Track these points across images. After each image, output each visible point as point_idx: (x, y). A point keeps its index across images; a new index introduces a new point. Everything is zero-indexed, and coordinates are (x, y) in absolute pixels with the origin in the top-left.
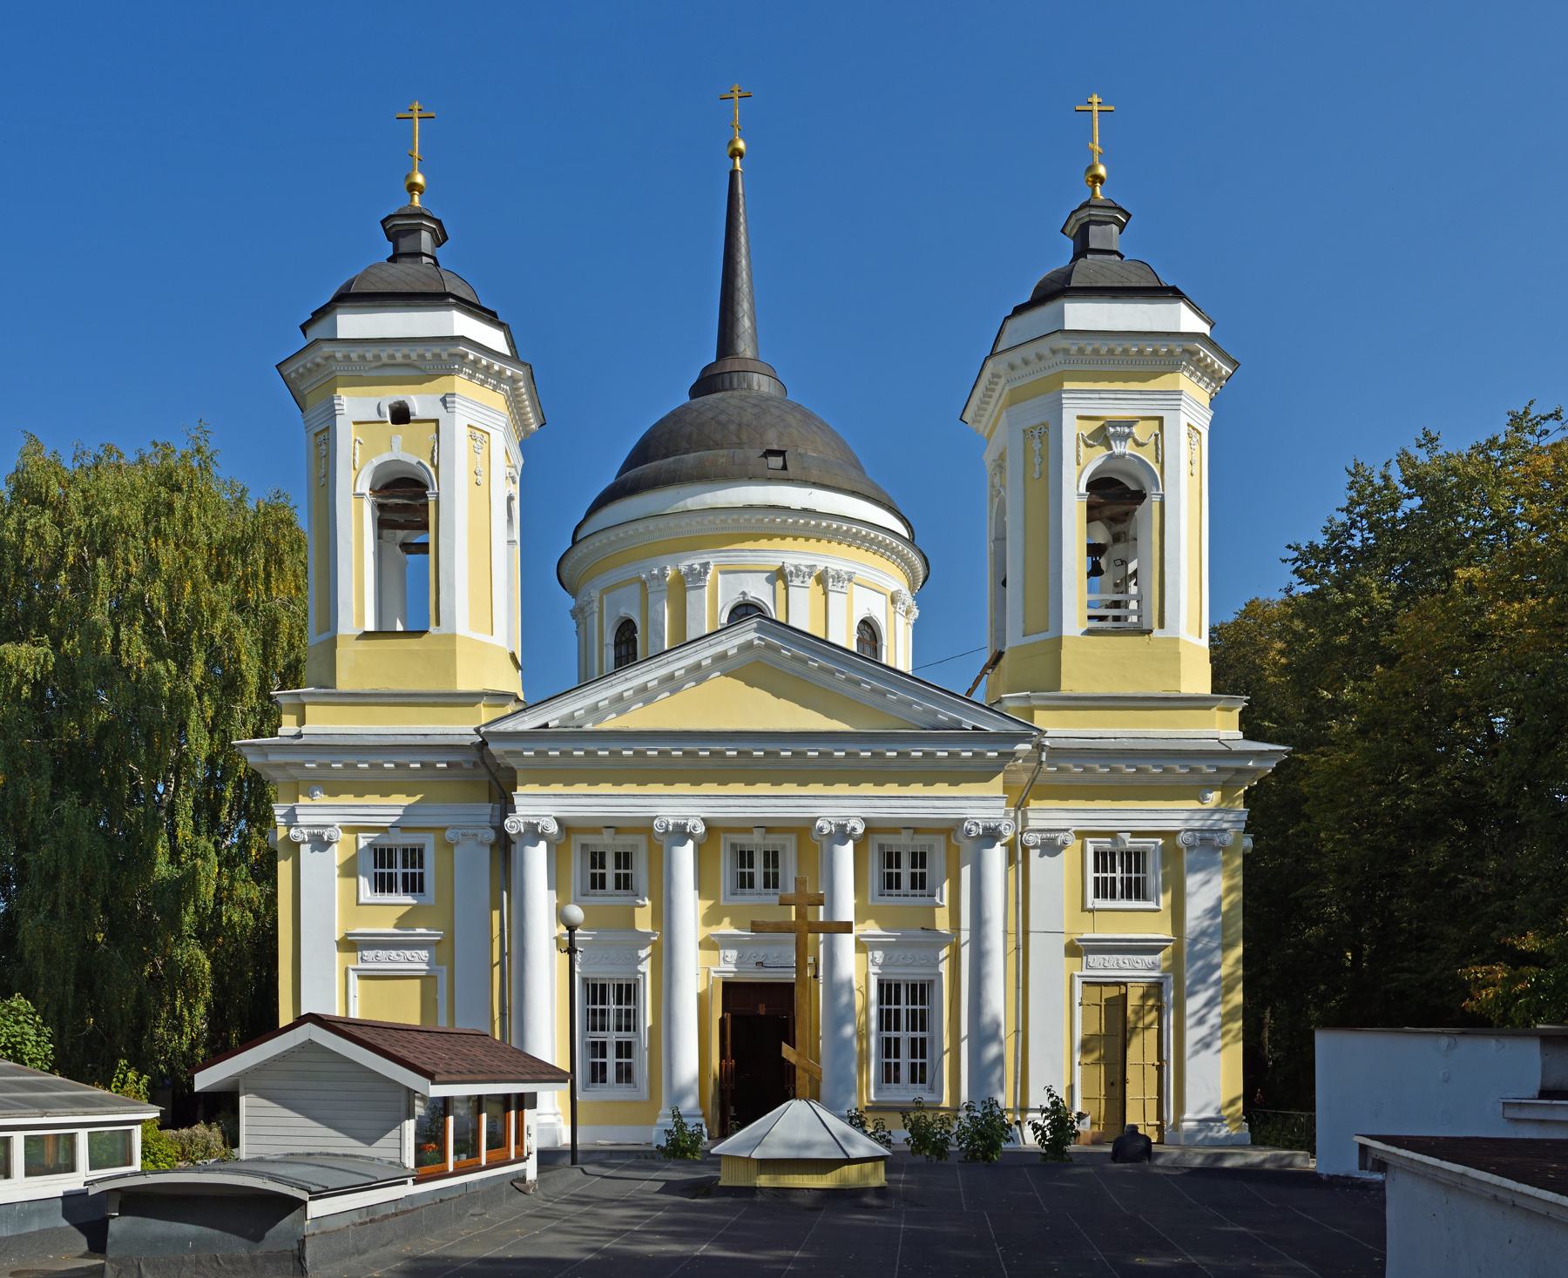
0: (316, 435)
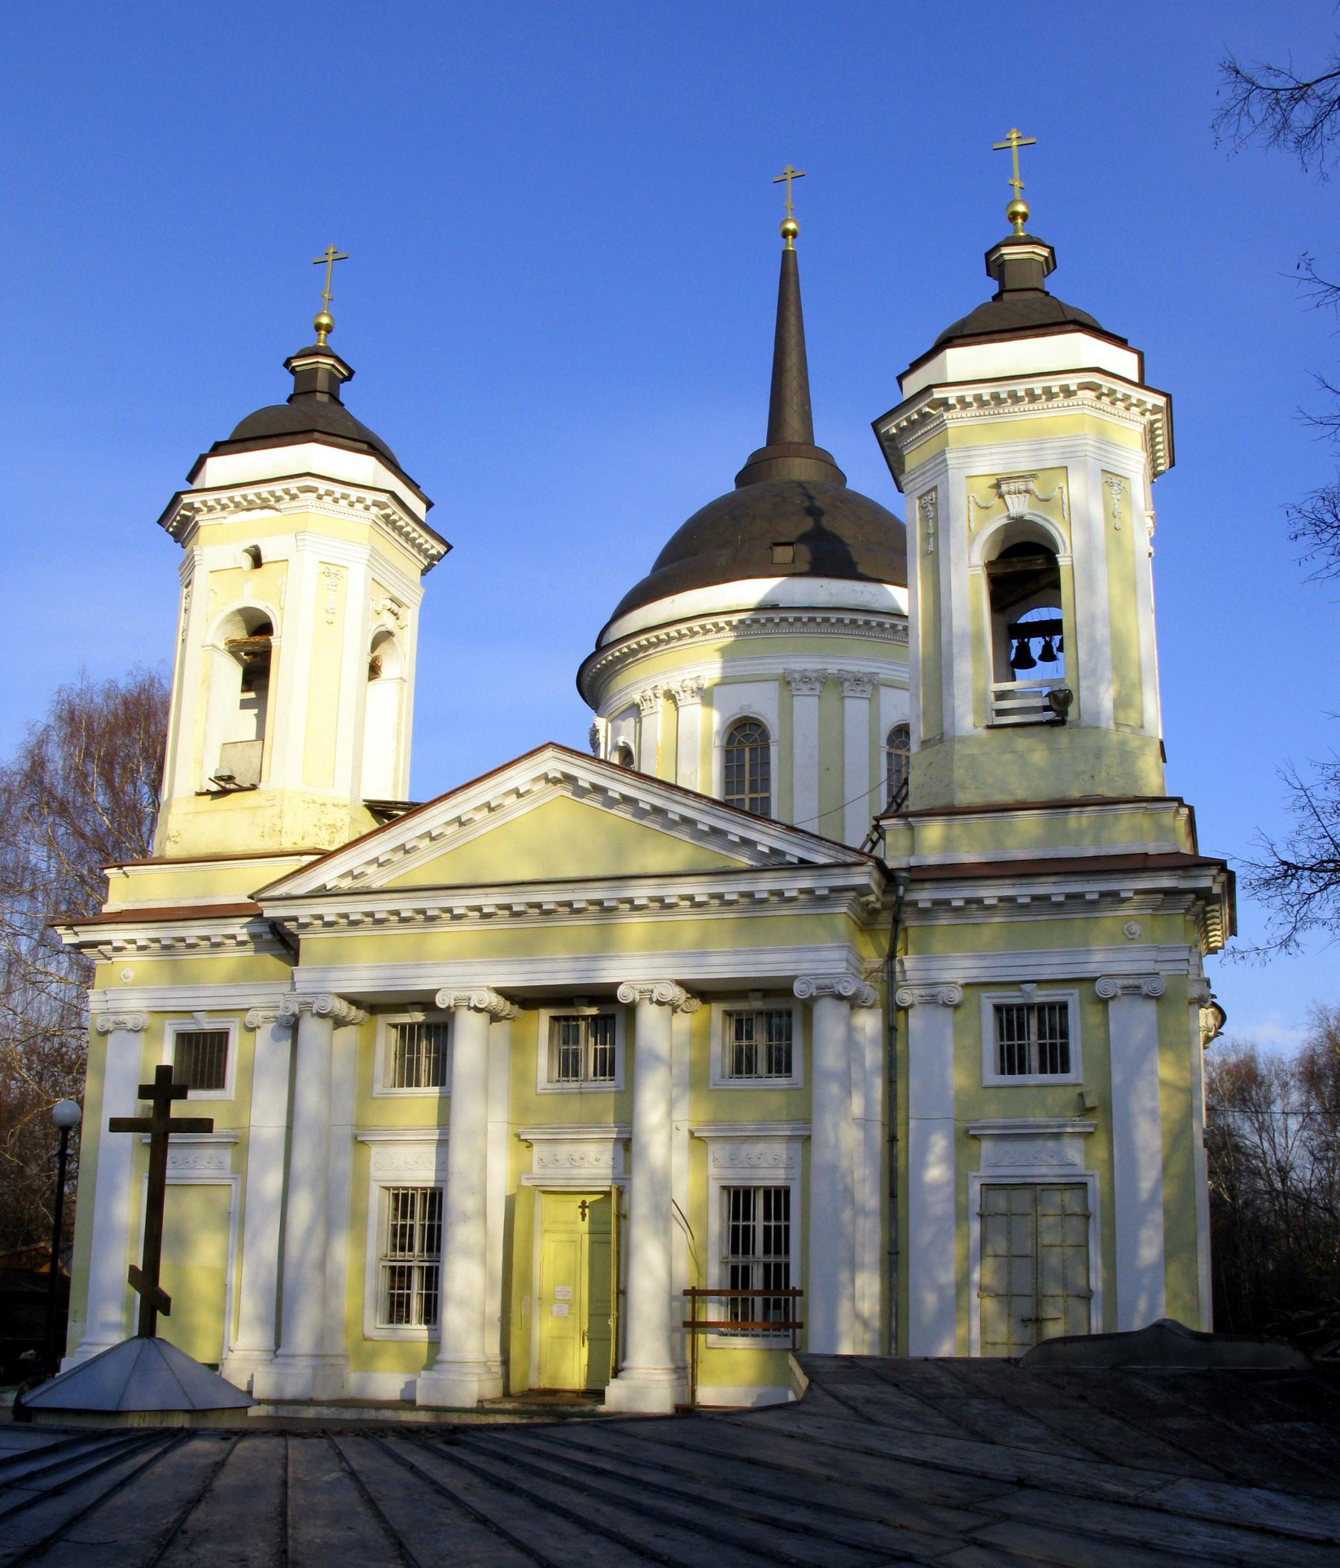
0: (920, 498)
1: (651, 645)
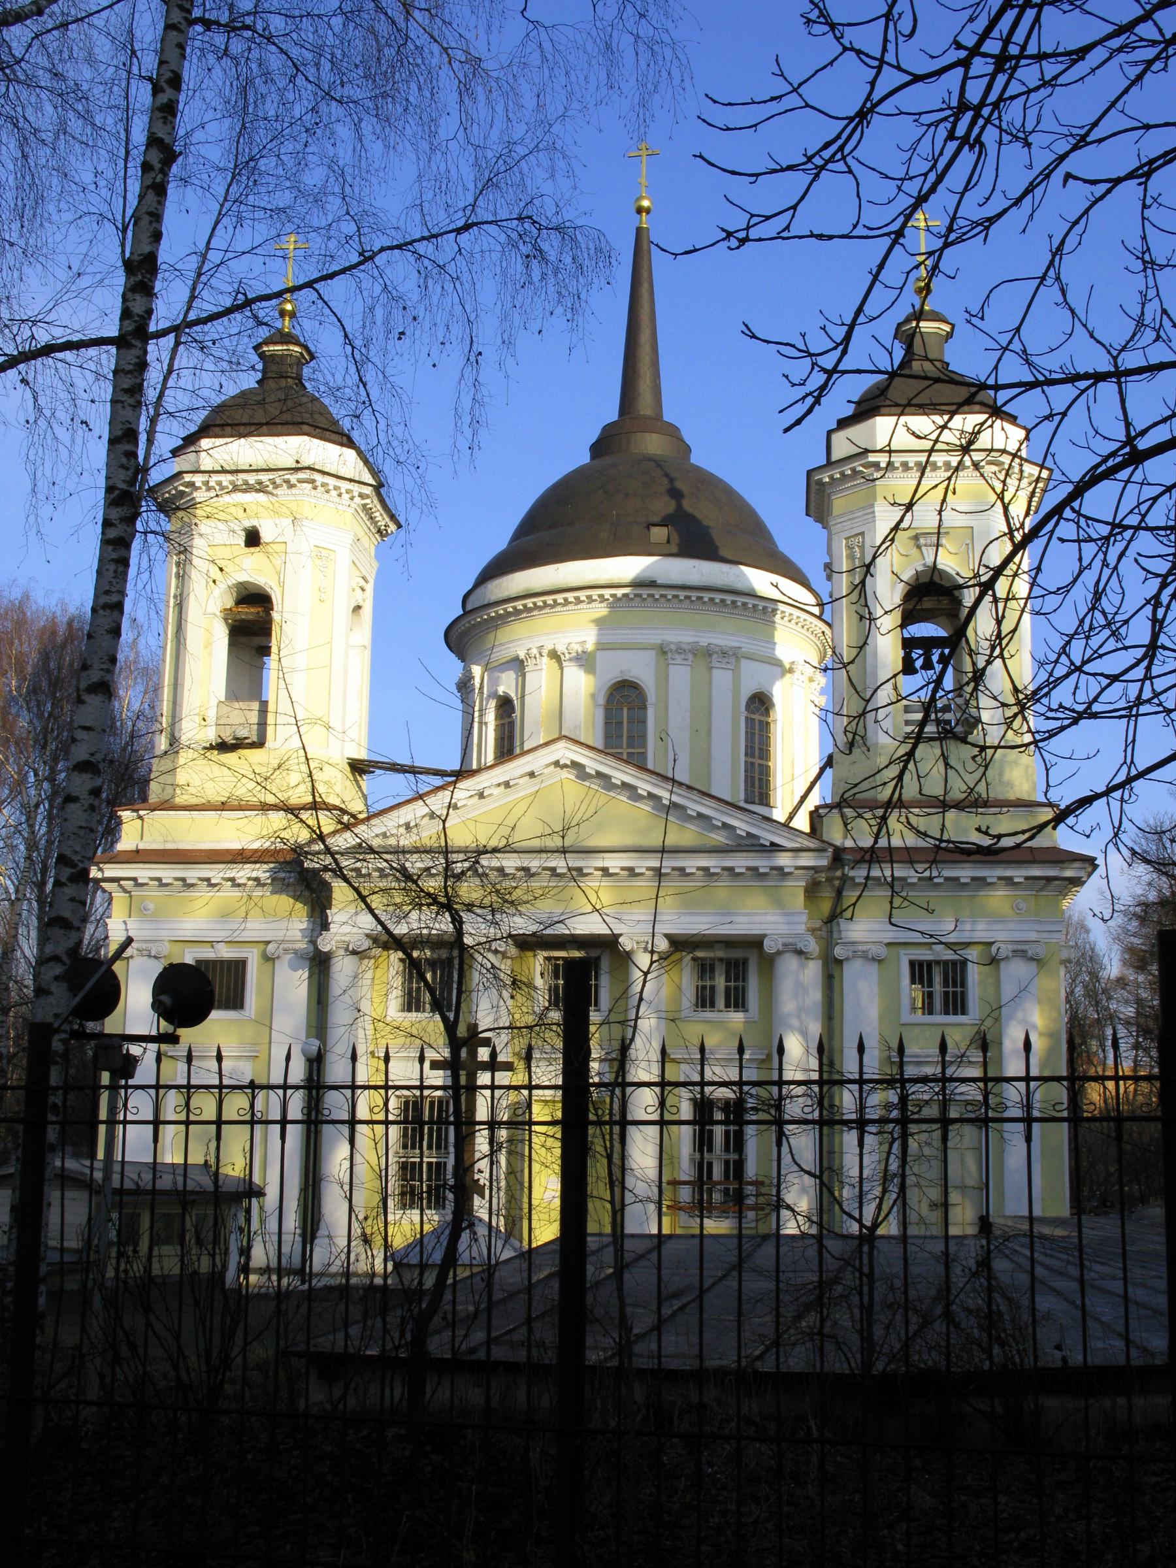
1: (536, 607)
